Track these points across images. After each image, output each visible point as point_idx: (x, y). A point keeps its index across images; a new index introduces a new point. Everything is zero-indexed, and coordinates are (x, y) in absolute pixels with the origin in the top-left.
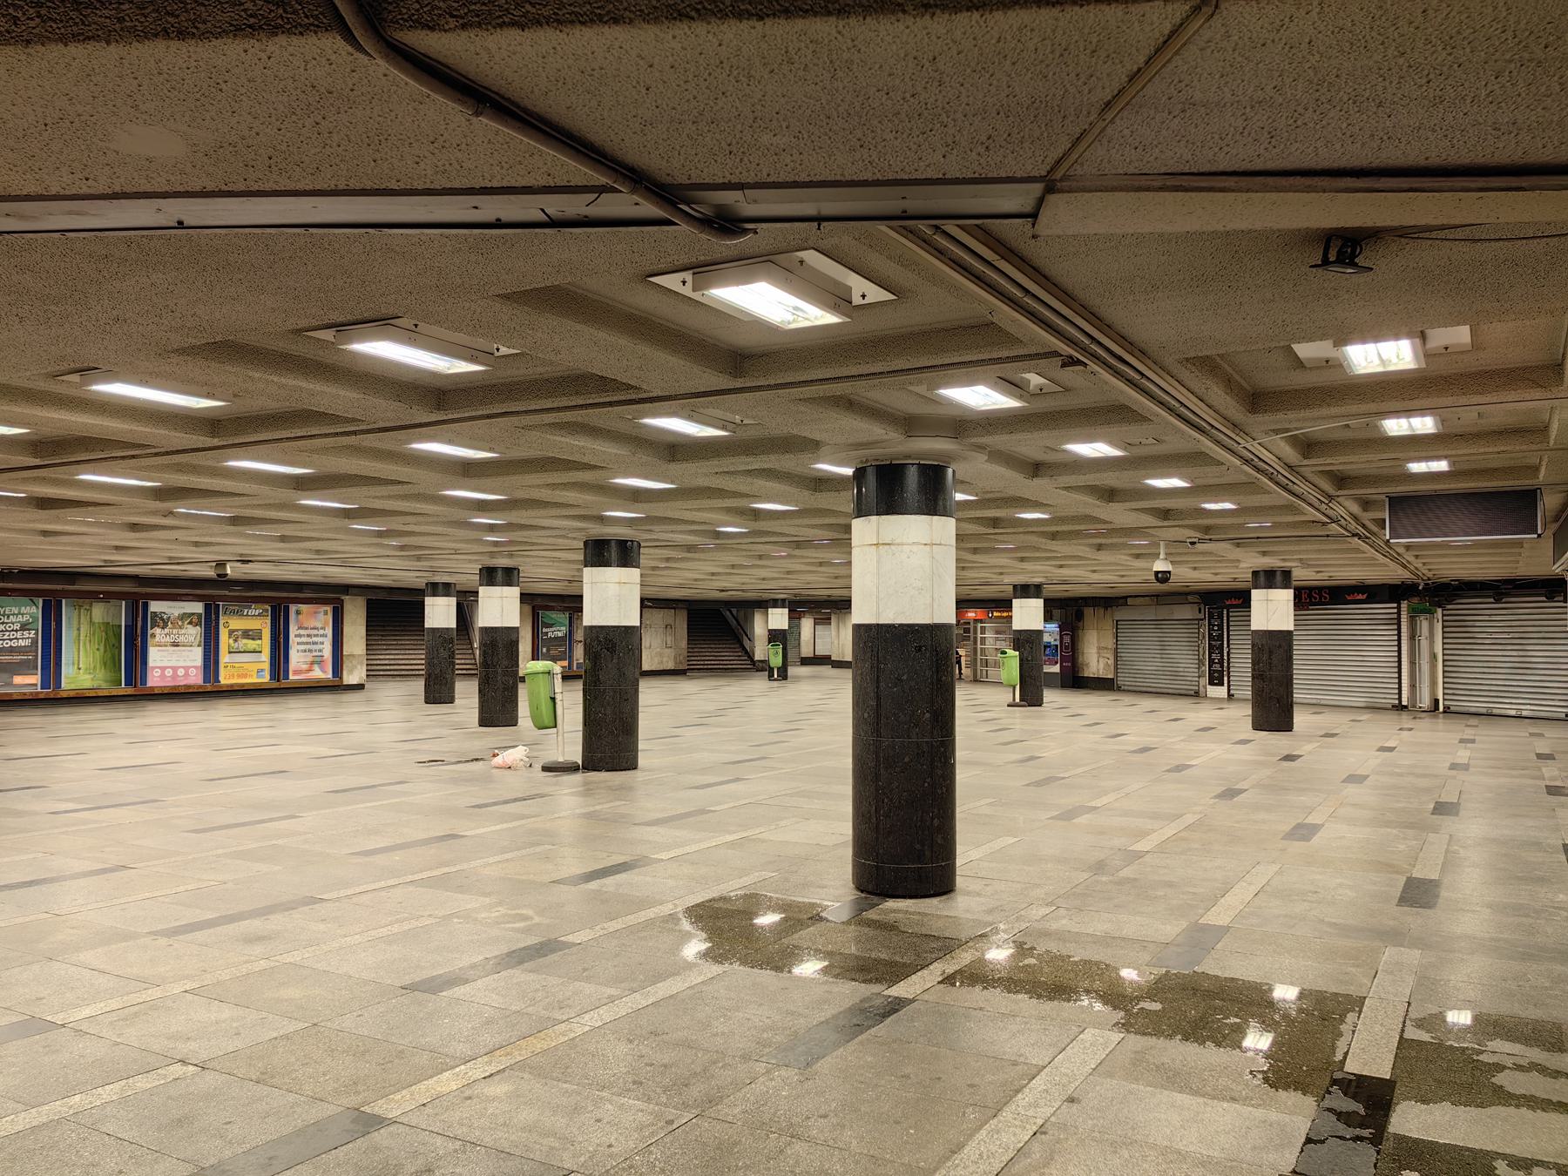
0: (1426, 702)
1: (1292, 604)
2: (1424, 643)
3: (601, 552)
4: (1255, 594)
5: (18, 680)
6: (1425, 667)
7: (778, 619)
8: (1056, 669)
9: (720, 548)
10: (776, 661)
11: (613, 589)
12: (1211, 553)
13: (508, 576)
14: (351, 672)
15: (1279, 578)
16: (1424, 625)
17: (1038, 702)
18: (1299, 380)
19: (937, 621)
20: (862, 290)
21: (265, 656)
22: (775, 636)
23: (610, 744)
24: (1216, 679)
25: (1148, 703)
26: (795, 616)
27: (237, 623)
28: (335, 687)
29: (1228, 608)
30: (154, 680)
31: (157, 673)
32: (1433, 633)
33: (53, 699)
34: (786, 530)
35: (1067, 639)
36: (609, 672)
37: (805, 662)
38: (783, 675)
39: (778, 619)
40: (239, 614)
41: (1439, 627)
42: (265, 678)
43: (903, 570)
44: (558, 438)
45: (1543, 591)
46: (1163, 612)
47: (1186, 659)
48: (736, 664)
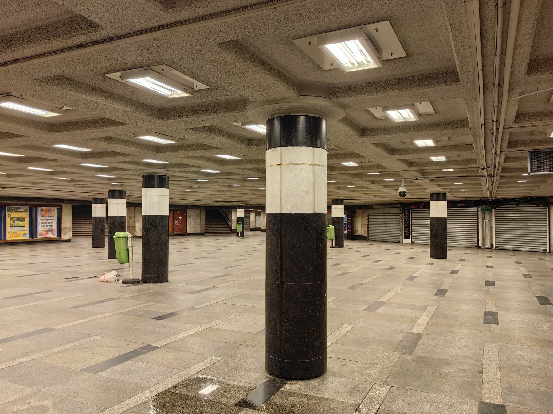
0: (488, 245)
1: (446, 207)
2: (487, 223)
3: (151, 181)
4: (432, 203)
6: (488, 232)
7: (240, 213)
9: (210, 182)
10: (240, 230)
11: (155, 198)
12: (389, 193)
13: (120, 194)
14: (65, 234)
16: (487, 216)
19: (317, 211)
21: (27, 228)
22: (239, 220)
23: (155, 269)
24: (407, 236)
25: (383, 246)
26: (247, 212)
27: (14, 215)
28: (58, 240)
29: (412, 209)
32: (491, 219)
34: (237, 171)
35: (350, 221)
36: (156, 237)
37: (252, 229)
38: (242, 235)
39: (240, 213)
40: (15, 211)
41: (493, 216)
42: (27, 237)
43: (296, 181)
44: (77, 94)
45: (535, 202)
46: (387, 211)
47: (394, 228)
48: (225, 231)
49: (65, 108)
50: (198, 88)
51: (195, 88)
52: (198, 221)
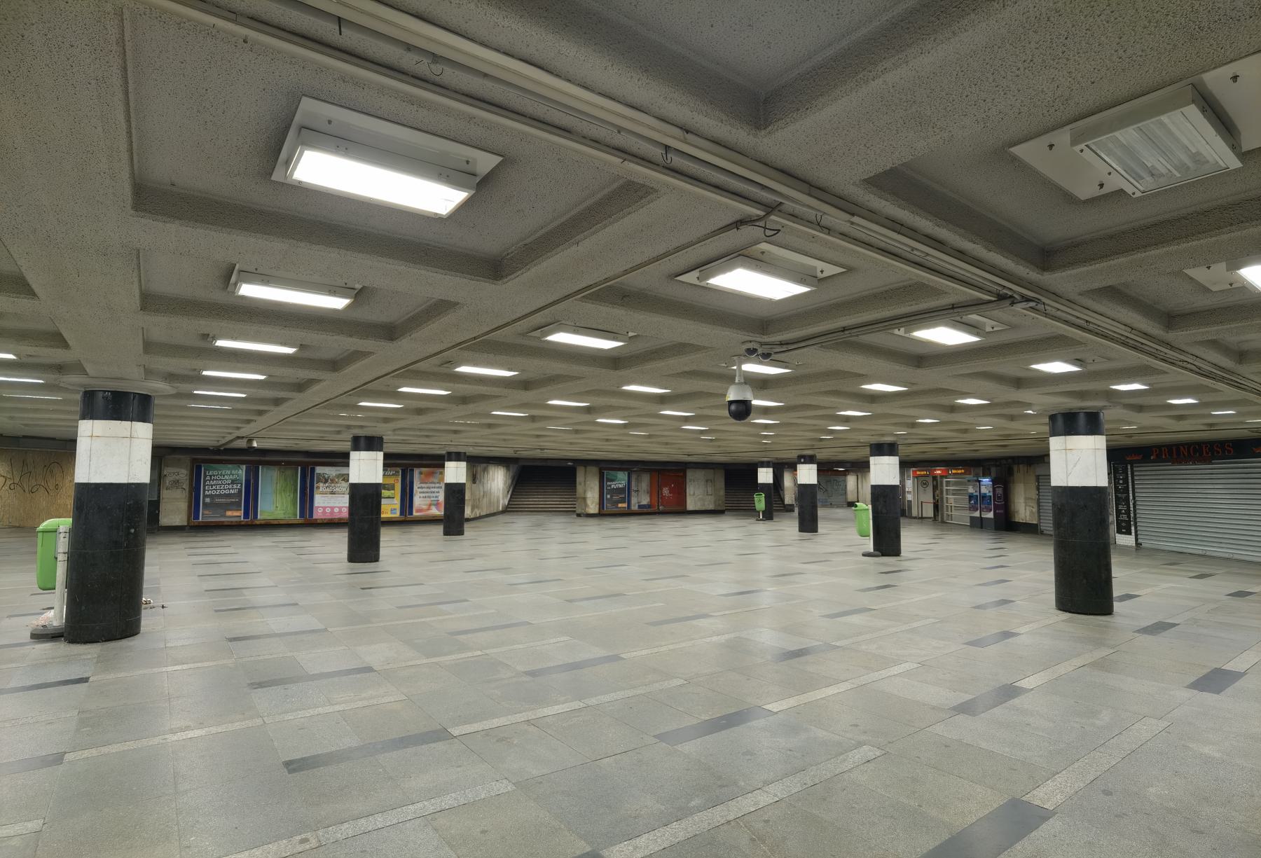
5: (229, 513)
8: (991, 515)
15: (1082, 421)
17: (895, 551)
18: (1202, 302)
20: (989, 325)
23: (103, 604)
30: (318, 514)
31: (320, 511)
33: (252, 525)
35: (1000, 491)
49: (631, 334)
50: (825, 274)
51: (820, 275)
52: (710, 490)
